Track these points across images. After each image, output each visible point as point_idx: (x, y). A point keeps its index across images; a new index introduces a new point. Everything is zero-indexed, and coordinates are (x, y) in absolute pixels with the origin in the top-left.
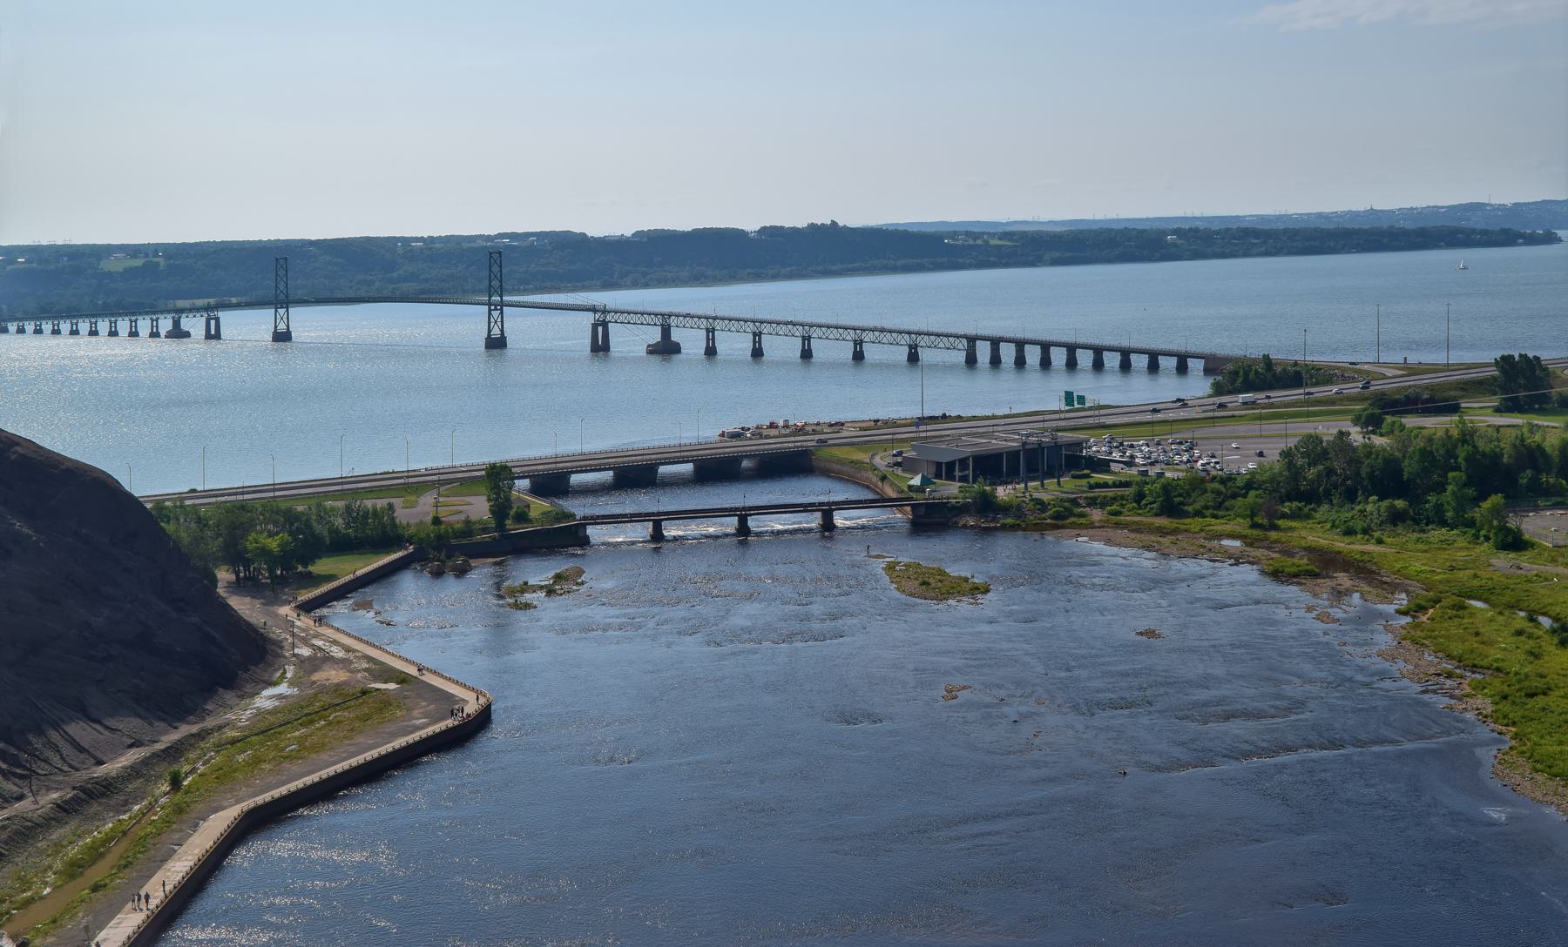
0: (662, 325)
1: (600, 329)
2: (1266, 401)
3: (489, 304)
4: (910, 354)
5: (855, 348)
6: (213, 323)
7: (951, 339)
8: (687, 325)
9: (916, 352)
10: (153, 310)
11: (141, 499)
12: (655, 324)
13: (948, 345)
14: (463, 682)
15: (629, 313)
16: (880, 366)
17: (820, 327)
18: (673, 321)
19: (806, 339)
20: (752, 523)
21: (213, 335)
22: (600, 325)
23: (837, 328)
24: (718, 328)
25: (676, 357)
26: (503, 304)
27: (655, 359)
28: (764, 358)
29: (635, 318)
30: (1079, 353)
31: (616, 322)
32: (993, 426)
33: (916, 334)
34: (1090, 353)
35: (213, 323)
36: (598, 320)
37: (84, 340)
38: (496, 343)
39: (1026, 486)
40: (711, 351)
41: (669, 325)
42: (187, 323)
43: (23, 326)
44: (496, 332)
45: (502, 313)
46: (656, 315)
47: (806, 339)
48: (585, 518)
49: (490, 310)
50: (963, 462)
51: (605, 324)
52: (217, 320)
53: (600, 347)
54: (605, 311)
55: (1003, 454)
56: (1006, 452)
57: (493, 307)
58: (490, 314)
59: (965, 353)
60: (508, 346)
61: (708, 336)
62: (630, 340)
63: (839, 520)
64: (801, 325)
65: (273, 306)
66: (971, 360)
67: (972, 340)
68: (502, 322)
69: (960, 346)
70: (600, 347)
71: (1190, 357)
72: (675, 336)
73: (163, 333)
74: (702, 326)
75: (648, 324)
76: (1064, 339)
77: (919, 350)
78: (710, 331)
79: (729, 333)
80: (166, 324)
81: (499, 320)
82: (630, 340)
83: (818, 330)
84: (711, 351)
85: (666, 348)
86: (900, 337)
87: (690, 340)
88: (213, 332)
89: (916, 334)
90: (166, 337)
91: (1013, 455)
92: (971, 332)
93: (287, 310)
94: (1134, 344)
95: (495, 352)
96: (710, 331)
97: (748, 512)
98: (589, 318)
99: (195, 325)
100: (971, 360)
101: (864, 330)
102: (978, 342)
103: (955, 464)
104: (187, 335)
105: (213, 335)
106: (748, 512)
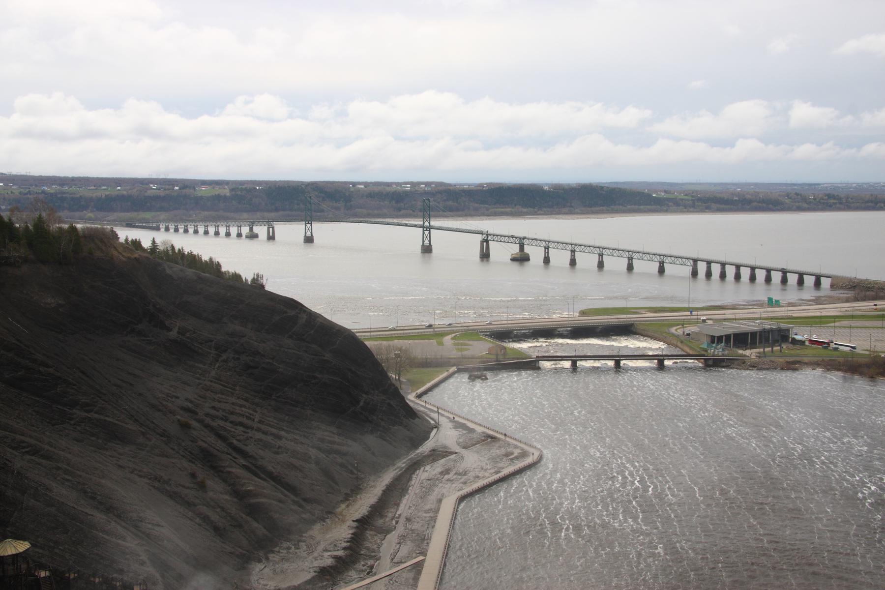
0: (519, 243)
1: (485, 244)
2: (874, 307)
3: (423, 227)
4: (660, 266)
5: (629, 261)
6: (271, 229)
7: (672, 258)
8: (534, 244)
9: (663, 266)
10: (239, 222)
11: (353, 331)
12: (516, 243)
13: (619, 255)
14: (520, 439)
15: (501, 236)
16: (673, 277)
17: (639, 253)
18: (526, 242)
19: (630, 259)
20: (578, 256)
21: (271, 238)
22: (484, 242)
23: (618, 250)
24: (635, 257)
25: (526, 263)
26: (429, 228)
27: (516, 264)
28: (209, 234)
29: (503, 239)
30: (757, 271)
31: (493, 240)
32: (841, 308)
33: (663, 256)
34: (749, 269)
35: (271, 229)
36: (484, 239)
37: (222, 240)
38: (309, 240)
39: (772, 349)
40: (547, 260)
41: (523, 244)
42: (256, 229)
43: (168, 226)
44: (309, 234)
45: (430, 233)
46: (516, 238)
47: (630, 259)
48: (538, 357)
49: (424, 231)
50: (728, 337)
51: (487, 241)
52: (273, 228)
53: (485, 256)
54: (488, 235)
55: (748, 333)
56: (717, 337)
57: (425, 229)
58: (424, 233)
59: (691, 268)
60: (314, 241)
61: (545, 251)
62: (501, 252)
63: (667, 363)
64: (599, 248)
65: (304, 222)
66: (695, 274)
67: (695, 261)
68: (430, 237)
69: (689, 264)
70: (485, 256)
71: (805, 274)
72: (527, 249)
73: (244, 234)
74: (542, 245)
75: (512, 243)
76: (780, 267)
77: (665, 264)
78: (573, 252)
79: (557, 250)
80: (245, 230)
81: (428, 236)
82: (501, 252)
83: (637, 254)
84: (547, 260)
85: (522, 259)
86: (623, 253)
87: (536, 253)
88: (271, 235)
89: (663, 256)
90: (247, 237)
91: (754, 334)
92: (695, 256)
93: (311, 225)
94: (758, 264)
95: (427, 255)
96: (573, 252)
97: (621, 358)
98: (479, 238)
99: (261, 230)
100: (695, 274)
101: (634, 252)
102: (712, 264)
103: (731, 336)
104: (256, 236)
105: (271, 238)
106: (621, 358)
